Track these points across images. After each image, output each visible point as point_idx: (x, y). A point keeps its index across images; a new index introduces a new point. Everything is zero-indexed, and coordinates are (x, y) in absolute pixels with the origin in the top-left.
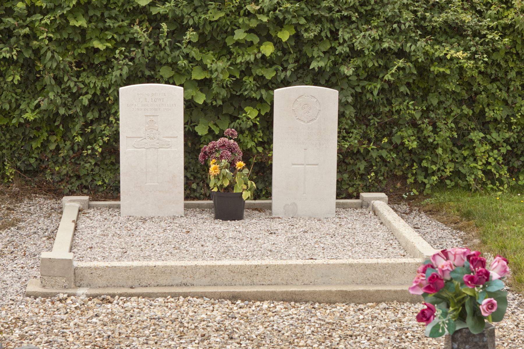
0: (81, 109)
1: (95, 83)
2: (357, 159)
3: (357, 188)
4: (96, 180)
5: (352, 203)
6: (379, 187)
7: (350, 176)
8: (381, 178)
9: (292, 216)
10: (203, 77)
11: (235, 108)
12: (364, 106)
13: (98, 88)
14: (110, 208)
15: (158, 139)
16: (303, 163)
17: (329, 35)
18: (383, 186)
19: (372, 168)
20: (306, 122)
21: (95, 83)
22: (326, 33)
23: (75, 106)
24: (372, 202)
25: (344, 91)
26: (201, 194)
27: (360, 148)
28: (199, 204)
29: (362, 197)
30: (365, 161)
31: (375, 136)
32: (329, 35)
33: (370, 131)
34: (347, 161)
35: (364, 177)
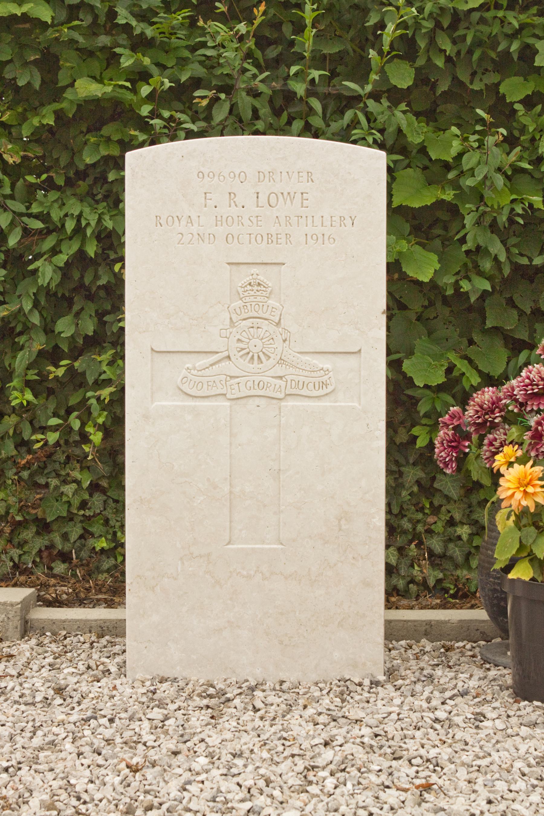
0: (36, 305)
1: (79, 217)
4: (92, 535)
10: (429, 201)
11: (522, 313)
13: (89, 232)
14: (101, 636)
15: (281, 361)
21: (79, 217)
23: (19, 296)
26: (412, 581)
28: (429, 623)
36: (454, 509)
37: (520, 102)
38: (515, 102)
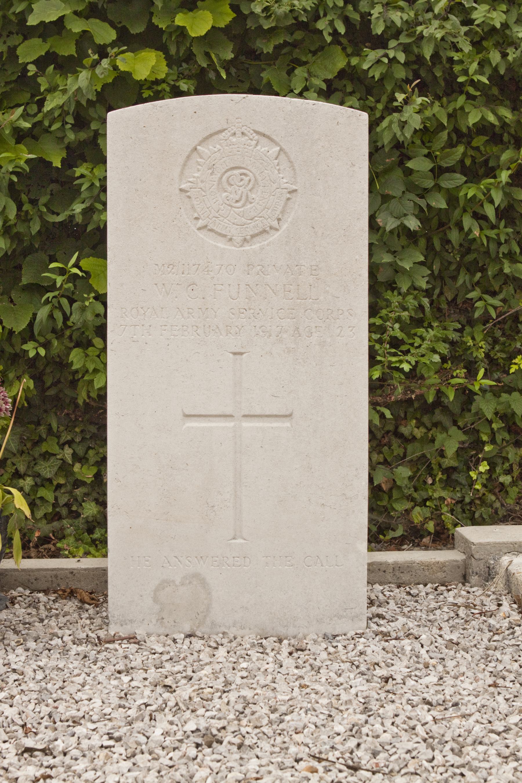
2: (436, 425)
3: (438, 508)
5: (428, 566)
6: (497, 505)
7: (415, 473)
8: (506, 479)
9: (187, 628)
12: (453, 267)
16: (228, 411)
17: (342, 30)
18: (510, 502)
19: (482, 450)
20: (238, 239)
22: (331, 23)
24: (505, 560)
25: (393, 204)
27: (443, 389)
29: (466, 541)
30: (459, 428)
31: (487, 355)
32: (342, 30)
33: (473, 338)
34: (405, 430)
35: (455, 476)
36: (19, 462)
37: (33, 63)
38: (28, 63)
